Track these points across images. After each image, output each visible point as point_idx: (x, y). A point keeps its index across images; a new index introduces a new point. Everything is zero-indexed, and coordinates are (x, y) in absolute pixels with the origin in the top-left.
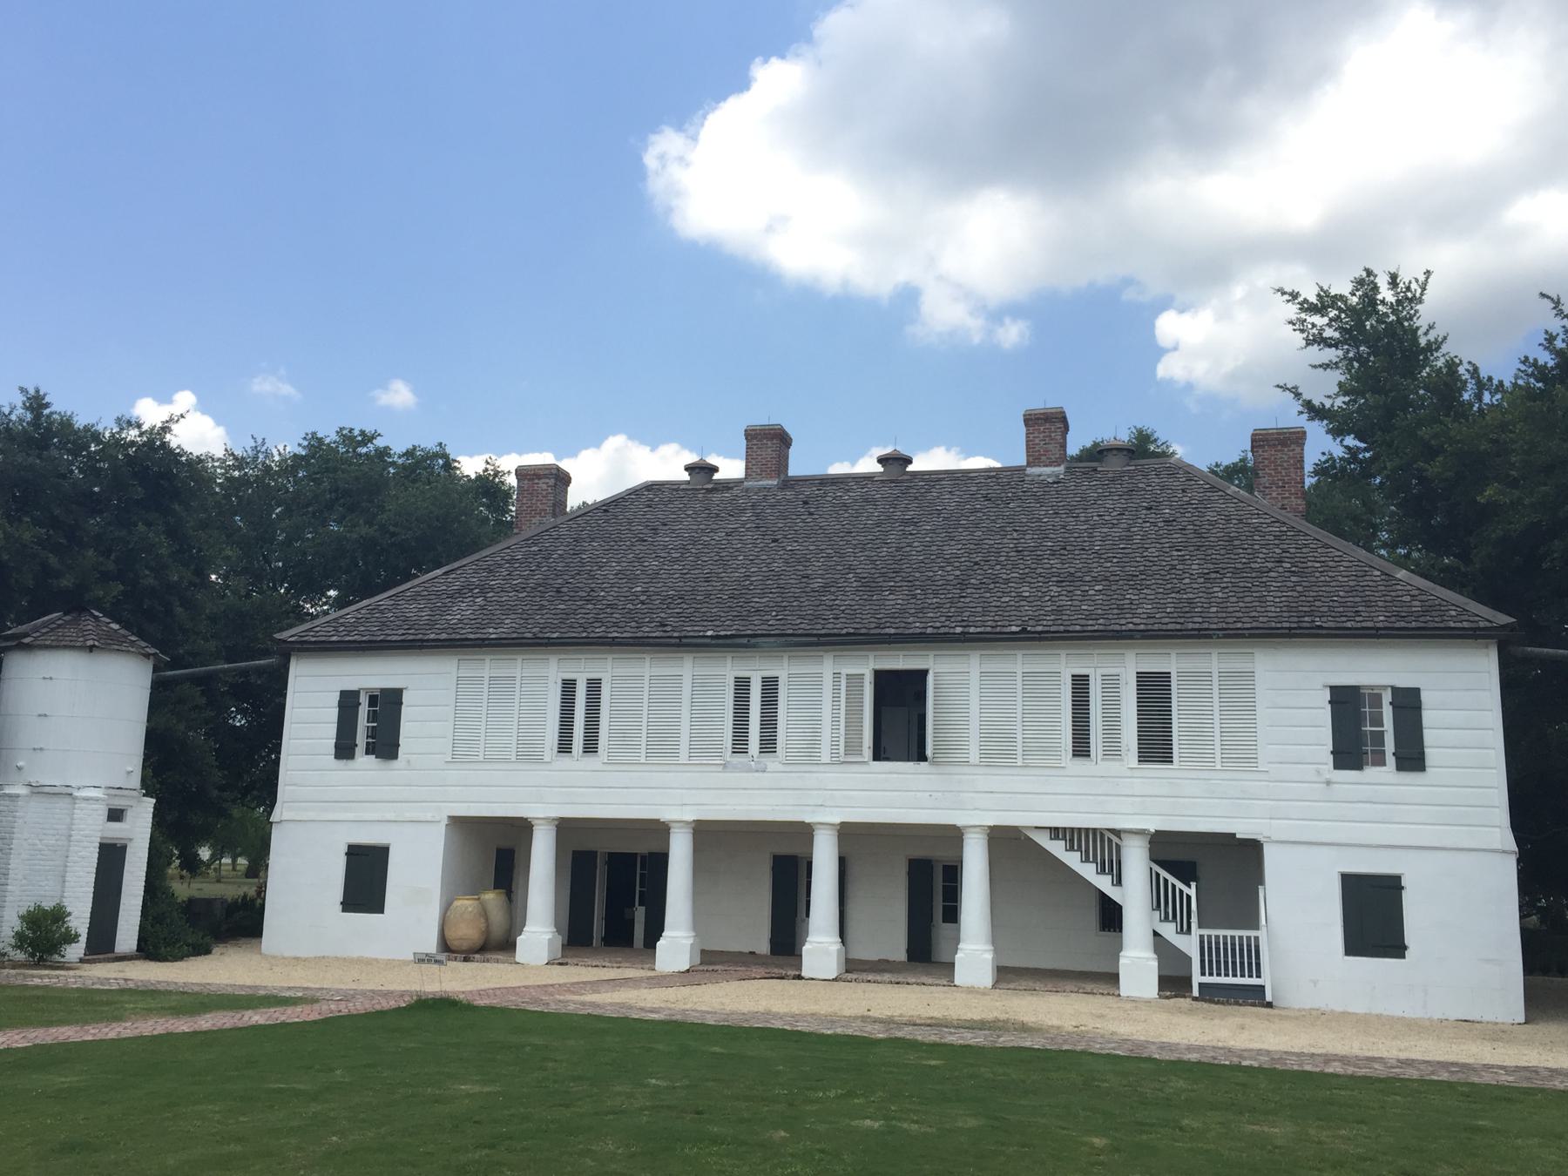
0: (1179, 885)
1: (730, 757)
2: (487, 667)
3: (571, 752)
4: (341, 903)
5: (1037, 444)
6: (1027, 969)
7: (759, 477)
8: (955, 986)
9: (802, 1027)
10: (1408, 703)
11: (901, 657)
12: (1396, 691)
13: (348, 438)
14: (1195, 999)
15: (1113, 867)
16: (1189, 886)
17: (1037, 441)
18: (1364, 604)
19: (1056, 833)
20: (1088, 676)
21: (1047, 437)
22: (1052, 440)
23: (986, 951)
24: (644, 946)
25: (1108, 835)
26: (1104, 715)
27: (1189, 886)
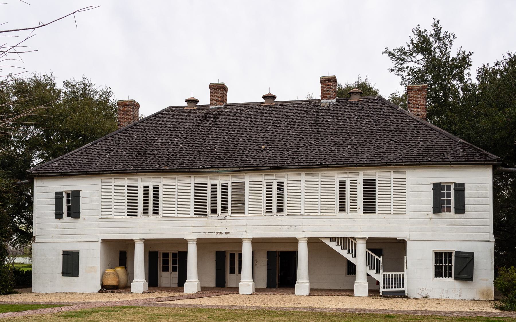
0: (376, 257)
5: (325, 90)
7: (215, 104)
15: (353, 252)
16: (380, 257)
17: (325, 89)
19: (332, 239)
22: (331, 89)
25: (351, 240)
27: (380, 257)
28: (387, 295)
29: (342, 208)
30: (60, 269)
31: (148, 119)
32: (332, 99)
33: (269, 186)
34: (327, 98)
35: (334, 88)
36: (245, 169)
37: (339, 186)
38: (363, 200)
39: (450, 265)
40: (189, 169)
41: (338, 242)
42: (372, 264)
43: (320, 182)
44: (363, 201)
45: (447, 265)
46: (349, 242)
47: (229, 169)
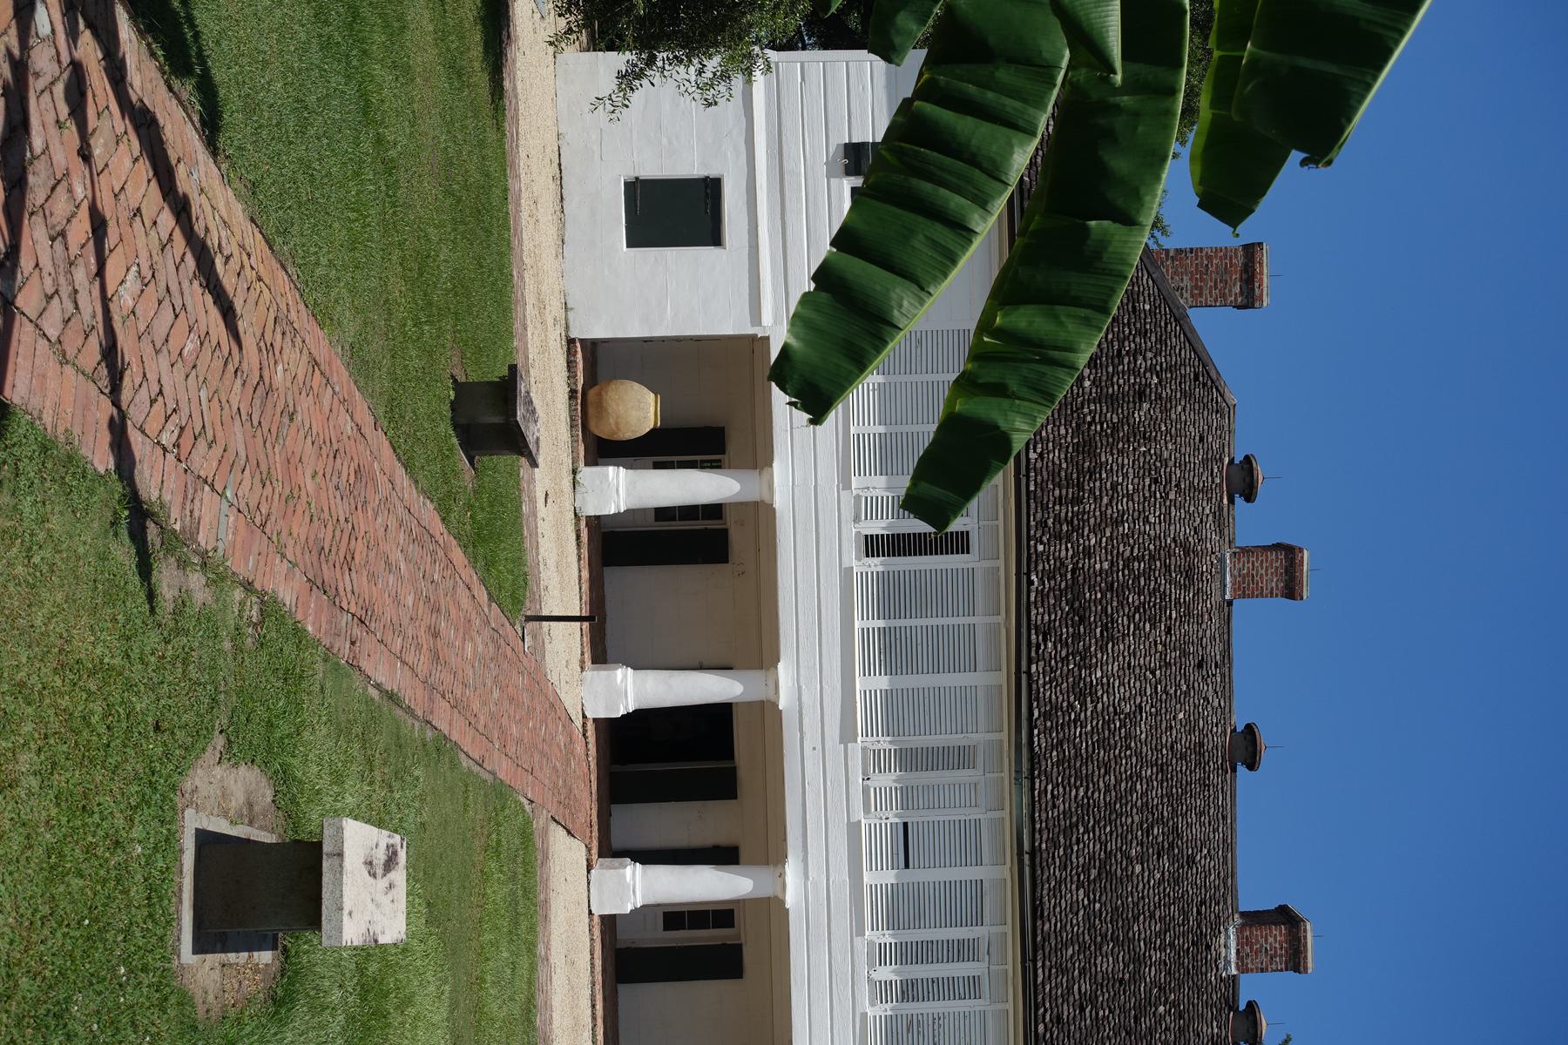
1: (858, 533)
3: (867, 556)
4: (637, 178)
5: (1266, 940)
6: (616, 1011)
7: (1236, 573)
11: (994, 736)
17: (1271, 940)
18: (1057, 451)
20: (968, 552)
21: (1276, 952)
22: (1272, 958)
23: (618, 506)
24: (604, 533)
26: (916, 691)
29: (907, 866)
30: (652, 170)
31: (1195, 353)
32: (1237, 964)
34: (1242, 947)
35: (1274, 967)
36: (1027, 870)
37: (947, 553)
38: (920, 534)
40: (1029, 673)
44: (915, 534)
47: (1026, 820)
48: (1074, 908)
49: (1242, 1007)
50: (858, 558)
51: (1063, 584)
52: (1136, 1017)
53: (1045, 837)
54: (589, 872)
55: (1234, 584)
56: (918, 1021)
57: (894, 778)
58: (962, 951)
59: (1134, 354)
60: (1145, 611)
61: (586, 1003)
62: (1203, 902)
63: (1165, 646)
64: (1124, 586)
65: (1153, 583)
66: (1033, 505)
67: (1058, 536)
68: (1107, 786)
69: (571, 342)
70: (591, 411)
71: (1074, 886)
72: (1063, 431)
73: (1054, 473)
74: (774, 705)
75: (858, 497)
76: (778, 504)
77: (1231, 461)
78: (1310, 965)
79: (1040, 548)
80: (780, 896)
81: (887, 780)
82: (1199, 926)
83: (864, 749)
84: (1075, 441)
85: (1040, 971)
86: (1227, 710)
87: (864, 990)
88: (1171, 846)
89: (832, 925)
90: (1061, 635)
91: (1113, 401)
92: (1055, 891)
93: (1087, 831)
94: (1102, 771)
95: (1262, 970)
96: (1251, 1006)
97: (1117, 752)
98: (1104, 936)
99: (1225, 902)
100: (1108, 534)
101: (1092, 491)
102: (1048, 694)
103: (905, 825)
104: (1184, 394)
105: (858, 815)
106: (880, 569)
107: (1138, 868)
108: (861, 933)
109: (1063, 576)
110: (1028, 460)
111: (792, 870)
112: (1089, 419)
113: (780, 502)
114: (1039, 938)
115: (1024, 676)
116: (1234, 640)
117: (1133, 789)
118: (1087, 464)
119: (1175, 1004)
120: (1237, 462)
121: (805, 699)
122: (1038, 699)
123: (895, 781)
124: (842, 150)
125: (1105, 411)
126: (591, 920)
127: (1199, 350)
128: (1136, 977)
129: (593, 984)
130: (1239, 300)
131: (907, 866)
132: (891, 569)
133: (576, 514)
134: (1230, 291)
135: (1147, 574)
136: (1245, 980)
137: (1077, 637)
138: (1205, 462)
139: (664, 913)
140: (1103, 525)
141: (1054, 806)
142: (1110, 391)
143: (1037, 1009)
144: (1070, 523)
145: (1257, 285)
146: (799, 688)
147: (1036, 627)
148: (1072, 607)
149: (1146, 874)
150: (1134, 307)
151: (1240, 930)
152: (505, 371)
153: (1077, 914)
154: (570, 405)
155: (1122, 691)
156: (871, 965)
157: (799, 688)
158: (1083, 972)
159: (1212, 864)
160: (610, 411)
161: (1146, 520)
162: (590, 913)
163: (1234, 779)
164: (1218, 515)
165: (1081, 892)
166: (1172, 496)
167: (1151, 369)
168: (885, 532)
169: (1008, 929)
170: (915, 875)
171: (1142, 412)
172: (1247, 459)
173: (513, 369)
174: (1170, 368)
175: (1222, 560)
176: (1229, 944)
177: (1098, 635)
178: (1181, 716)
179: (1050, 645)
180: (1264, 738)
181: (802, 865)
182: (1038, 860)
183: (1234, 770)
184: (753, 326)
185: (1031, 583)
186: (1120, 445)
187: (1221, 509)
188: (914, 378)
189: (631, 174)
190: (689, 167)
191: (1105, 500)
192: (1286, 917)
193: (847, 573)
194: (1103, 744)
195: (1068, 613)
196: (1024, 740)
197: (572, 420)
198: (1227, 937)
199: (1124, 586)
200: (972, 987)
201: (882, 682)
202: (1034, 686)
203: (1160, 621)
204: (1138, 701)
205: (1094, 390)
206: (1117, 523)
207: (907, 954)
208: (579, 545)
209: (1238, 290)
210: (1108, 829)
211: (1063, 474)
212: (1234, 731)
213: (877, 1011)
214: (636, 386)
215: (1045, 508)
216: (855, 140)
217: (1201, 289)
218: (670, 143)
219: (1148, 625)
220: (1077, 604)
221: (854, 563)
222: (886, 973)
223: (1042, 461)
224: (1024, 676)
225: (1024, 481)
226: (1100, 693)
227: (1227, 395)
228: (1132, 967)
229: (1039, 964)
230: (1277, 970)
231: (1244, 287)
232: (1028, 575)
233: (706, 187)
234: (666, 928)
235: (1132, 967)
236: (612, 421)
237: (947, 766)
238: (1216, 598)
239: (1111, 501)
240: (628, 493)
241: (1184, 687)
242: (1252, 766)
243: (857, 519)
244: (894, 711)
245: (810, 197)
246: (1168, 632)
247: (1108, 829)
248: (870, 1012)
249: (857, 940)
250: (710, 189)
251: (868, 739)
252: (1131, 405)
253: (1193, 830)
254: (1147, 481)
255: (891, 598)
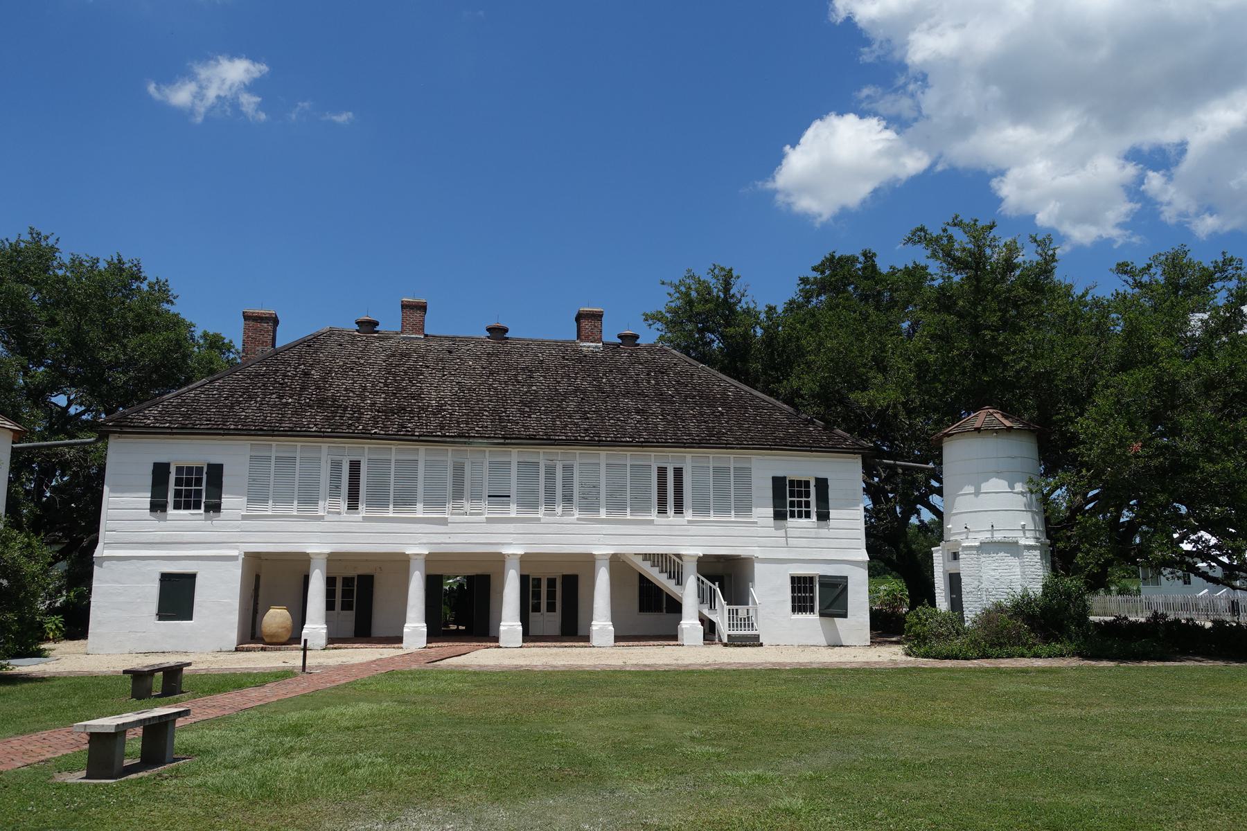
0: (712, 585)
1: (346, 513)
2: (276, 447)
7: (411, 332)
8: (594, 647)
9: (691, 668)
10: (822, 484)
12: (817, 480)
13: (117, 267)
14: (725, 645)
15: (678, 578)
16: (715, 585)
19: (646, 557)
25: (673, 557)
27: (715, 585)
28: (734, 642)
29: (509, 496)
30: (154, 607)
33: (662, 472)
36: (513, 441)
39: (811, 595)
40: (419, 436)
41: (654, 562)
42: (706, 597)
43: (732, 471)
45: (803, 595)
46: (670, 563)
47: (490, 441)
48: (538, 420)
49: (620, 341)
50: (359, 513)
51: (383, 417)
52: (602, 393)
53: (499, 432)
54: (501, 647)
55: (416, 333)
56: (583, 494)
57: (343, 503)
58: (550, 472)
59: (285, 376)
60: (413, 378)
61: (569, 650)
62: (563, 357)
63: (434, 369)
64: (397, 388)
65: (402, 373)
66: (338, 430)
67: (359, 419)
68: (489, 401)
69: (237, 650)
70: (274, 640)
71: (529, 419)
72: (309, 414)
73: (327, 419)
74: (522, 556)
75: (329, 512)
76: (329, 551)
77: (357, 331)
78: (599, 310)
79: (361, 427)
80: (519, 556)
81: (467, 506)
82: (573, 360)
83: (452, 514)
84: (316, 407)
85: (560, 438)
86: (478, 340)
87: (566, 518)
88: (530, 371)
89: (534, 532)
90: (407, 419)
91: (303, 388)
92: (526, 428)
93: (505, 412)
94: (480, 403)
95: (601, 332)
96: (620, 337)
97: (474, 395)
98: (559, 406)
99: (568, 346)
100: (368, 394)
101: (344, 401)
102: (432, 427)
103: (489, 496)
104: (315, 352)
105: (483, 518)
106: (365, 505)
107: (534, 388)
108: (539, 519)
109: (379, 417)
110: (315, 431)
111: (506, 551)
112: (308, 401)
113: (327, 549)
114: (545, 437)
115: (421, 438)
116: (445, 335)
117: (496, 389)
118: (330, 403)
119: (604, 375)
120: (358, 328)
121: (425, 541)
122: (432, 432)
123: (468, 502)
124: (154, 514)
125: (307, 393)
126: (525, 647)
127: (296, 343)
128: (584, 392)
129: (555, 646)
130: (270, 324)
131: (509, 496)
132: (365, 500)
133: (324, 649)
134: (266, 328)
135: (395, 375)
136: (606, 339)
137: (411, 412)
138: (352, 344)
139: (547, 611)
140: (363, 396)
141: (486, 427)
142: (298, 389)
143: (578, 440)
144: (355, 412)
145: (264, 316)
146: (420, 544)
147: (398, 431)
148: (396, 414)
149: (538, 384)
150: (261, 375)
151: (582, 341)
152: (128, 676)
153: (542, 418)
154: (269, 651)
155: (446, 391)
156: (555, 515)
157: (420, 544)
158: (570, 417)
159: (547, 352)
160: (275, 631)
161: (369, 375)
162: (521, 647)
163: (511, 339)
164: (381, 339)
165: (532, 416)
166: (362, 361)
167: (296, 368)
168: (347, 502)
169: (541, 451)
170: (513, 493)
171: (315, 374)
172: (357, 323)
173: (125, 672)
174: (299, 359)
175: (404, 338)
176: (587, 346)
177: (415, 401)
178: (471, 363)
179: (409, 425)
180: (493, 324)
181: (505, 546)
182: (509, 436)
183: (507, 338)
184: (238, 560)
185: (375, 433)
186: (327, 386)
187: (380, 337)
188: (272, 483)
189: (154, 617)
190: (153, 590)
191: (351, 394)
192: (580, 317)
193: (365, 519)
194: (467, 402)
195: (398, 416)
196: (452, 440)
197: (277, 650)
198: (584, 346)
199: (397, 388)
200: (568, 469)
201: (420, 506)
202: (425, 434)
203: (421, 370)
204: (454, 383)
205: (295, 397)
206: (365, 389)
207: (550, 501)
208: (340, 648)
209: (266, 324)
210: (509, 401)
211: (329, 415)
212: (489, 337)
213: (577, 514)
214: (265, 618)
215: (342, 424)
216: (772, 516)
217: (263, 342)
218: (140, 598)
219: (421, 377)
220: (396, 411)
221: (361, 515)
222: (559, 510)
223: (318, 424)
224: (421, 438)
225: (325, 434)
226: (443, 402)
227: (324, 331)
228: (578, 394)
229: (557, 438)
230: (601, 325)
231: (264, 321)
232: (372, 434)
233: (165, 580)
234: (555, 611)
235: (578, 394)
236: (280, 630)
237: (463, 476)
238: (422, 343)
239: (352, 392)
240: (316, 623)
241: (458, 360)
242: (506, 330)
243: (339, 513)
244: (434, 501)
245: (177, 529)
246: (428, 367)
247: (509, 401)
248: (577, 516)
249: (542, 521)
250: (166, 578)
251: (447, 511)
252: (310, 379)
253: (527, 361)
254: (350, 373)
255: (379, 500)
